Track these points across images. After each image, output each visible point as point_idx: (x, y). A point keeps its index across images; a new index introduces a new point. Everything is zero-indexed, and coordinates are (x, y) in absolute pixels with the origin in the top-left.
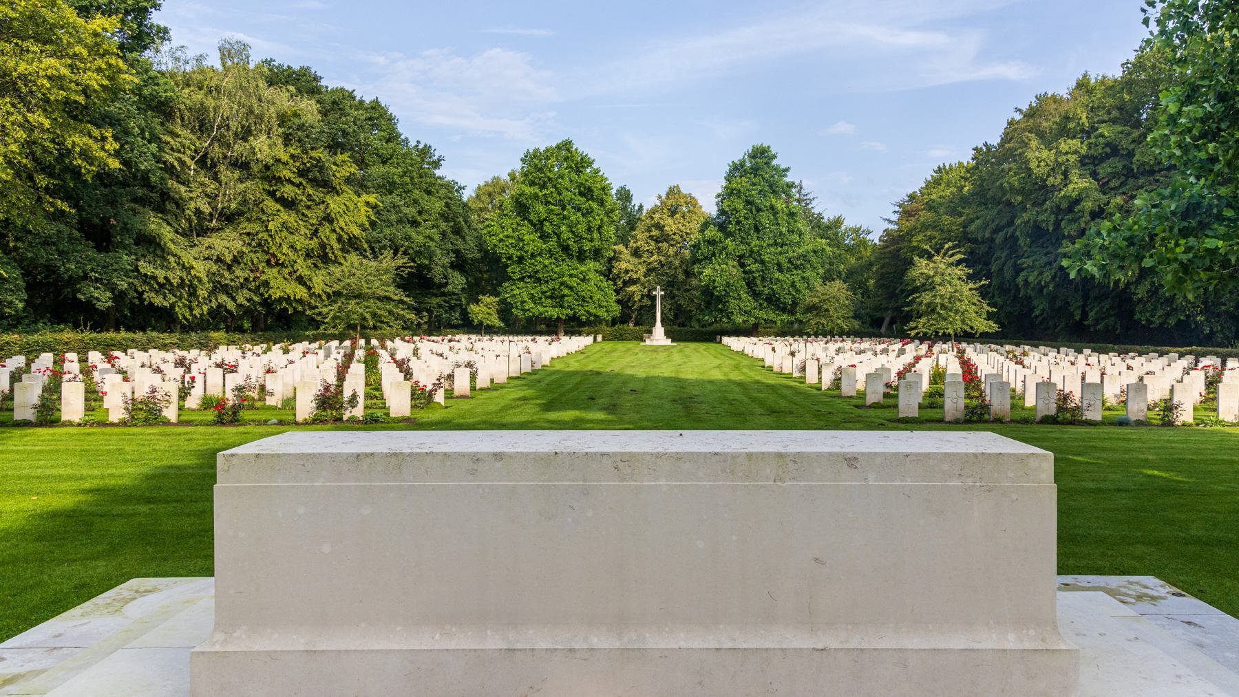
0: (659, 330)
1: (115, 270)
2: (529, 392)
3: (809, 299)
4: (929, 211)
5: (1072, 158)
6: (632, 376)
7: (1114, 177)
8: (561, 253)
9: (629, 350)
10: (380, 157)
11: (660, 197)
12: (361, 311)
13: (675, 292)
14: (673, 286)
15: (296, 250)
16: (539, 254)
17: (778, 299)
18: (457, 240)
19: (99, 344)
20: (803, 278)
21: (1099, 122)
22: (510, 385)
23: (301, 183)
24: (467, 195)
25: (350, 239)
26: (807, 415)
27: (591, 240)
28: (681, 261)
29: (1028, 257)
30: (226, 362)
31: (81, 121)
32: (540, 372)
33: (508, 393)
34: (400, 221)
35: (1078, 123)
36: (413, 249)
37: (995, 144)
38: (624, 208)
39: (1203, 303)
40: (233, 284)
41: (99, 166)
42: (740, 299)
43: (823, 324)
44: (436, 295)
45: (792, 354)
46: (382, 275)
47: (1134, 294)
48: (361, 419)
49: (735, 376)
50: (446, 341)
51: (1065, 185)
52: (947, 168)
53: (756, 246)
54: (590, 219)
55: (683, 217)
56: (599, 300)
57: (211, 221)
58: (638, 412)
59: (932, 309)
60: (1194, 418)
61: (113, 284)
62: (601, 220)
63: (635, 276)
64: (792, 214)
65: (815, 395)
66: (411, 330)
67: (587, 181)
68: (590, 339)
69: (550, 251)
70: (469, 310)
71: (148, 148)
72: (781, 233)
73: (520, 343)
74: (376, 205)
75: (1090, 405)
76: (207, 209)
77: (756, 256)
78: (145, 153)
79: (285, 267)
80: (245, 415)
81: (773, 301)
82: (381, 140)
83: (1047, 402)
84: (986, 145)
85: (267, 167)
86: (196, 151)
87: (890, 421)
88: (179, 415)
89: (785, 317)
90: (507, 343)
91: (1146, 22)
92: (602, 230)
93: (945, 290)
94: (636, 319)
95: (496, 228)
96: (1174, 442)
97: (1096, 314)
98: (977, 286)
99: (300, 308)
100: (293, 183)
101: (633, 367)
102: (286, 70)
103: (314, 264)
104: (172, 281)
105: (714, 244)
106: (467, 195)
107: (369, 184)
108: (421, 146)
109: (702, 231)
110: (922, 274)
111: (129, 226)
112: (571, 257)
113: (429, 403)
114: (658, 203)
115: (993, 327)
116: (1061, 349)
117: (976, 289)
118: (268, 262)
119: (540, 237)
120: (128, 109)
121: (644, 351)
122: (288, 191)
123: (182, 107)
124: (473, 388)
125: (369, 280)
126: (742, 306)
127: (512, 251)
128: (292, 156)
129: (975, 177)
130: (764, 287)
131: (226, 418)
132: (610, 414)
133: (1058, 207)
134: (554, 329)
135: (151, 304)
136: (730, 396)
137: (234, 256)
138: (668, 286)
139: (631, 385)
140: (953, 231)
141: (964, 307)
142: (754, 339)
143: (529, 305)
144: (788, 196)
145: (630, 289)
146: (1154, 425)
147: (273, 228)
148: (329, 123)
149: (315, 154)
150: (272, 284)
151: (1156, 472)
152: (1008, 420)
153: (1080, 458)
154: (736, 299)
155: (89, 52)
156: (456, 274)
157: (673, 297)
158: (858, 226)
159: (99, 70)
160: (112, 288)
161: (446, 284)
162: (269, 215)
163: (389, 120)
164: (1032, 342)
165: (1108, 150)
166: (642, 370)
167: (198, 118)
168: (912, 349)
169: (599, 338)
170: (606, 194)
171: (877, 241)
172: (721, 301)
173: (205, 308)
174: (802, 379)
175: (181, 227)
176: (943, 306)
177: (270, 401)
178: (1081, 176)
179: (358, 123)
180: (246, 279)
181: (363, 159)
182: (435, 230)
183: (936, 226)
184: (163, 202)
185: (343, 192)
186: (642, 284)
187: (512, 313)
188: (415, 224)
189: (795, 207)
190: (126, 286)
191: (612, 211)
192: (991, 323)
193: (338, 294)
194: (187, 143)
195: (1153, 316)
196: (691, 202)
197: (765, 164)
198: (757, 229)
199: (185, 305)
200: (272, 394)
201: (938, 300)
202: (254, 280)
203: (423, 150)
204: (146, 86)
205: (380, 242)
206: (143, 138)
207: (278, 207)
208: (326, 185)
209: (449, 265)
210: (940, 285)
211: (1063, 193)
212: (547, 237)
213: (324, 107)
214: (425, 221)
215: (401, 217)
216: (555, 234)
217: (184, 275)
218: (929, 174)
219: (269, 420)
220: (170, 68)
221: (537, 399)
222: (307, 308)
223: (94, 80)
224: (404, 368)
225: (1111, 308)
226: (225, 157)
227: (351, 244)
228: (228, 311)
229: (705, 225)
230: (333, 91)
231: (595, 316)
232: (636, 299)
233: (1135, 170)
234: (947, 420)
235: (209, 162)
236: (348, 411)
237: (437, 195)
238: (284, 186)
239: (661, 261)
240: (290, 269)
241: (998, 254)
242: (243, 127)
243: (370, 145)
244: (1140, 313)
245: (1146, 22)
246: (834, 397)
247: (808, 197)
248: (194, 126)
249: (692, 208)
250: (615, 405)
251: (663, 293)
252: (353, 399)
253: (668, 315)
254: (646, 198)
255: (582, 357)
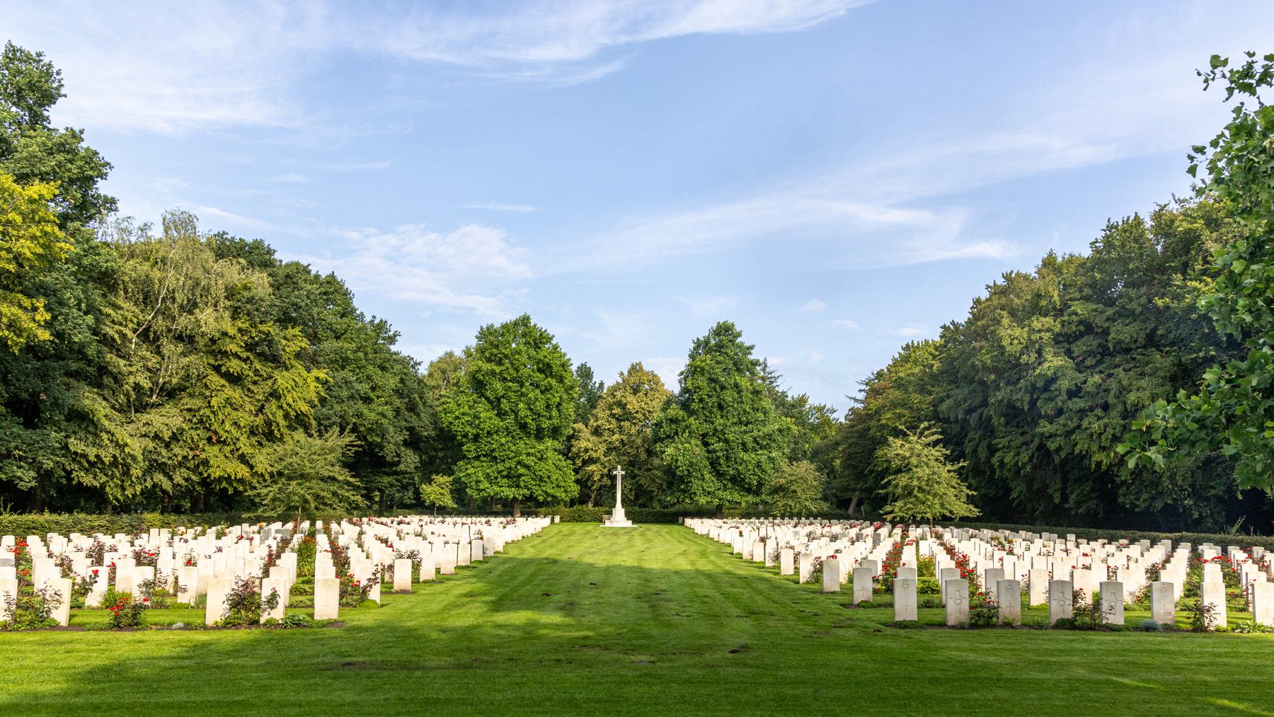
0: (619, 511)
1: (41, 448)
2: (479, 586)
3: (775, 480)
4: (898, 389)
5: (1046, 336)
6: (591, 565)
7: (1090, 356)
8: (518, 431)
9: (588, 532)
10: (334, 331)
11: (622, 374)
12: (302, 492)
13: (636, 472)
14: (633, 466)
15: (239, 427)
16: (496, 432)
17: (743, 480)
18: (411, 417)
19: (19, 527)
20: (769, 457)
21: (1071, 300)
22: (459, 576)
23: (248, 358)
24: (423, 371)
25: (298, 415)
26: (790, 617)
27: (550, 418)
28: (643, 440)
29: (1003, 437)
30: (147, 550)
31: (12, 291)
32: (491, 560)
33: (453, 587)
34: (352, 397)
35: (1050, 301)
36: (364, 426)
37: (963, 323)
38: (585, 386)
39: (1190, 486)
40: (170, 462)
41: (28, 337)
42: (703, 479)
43: (791, 506)
44: (388, 474)
45: (763, 540)
46: (328, 454)
47: (1117, 476)
48: (280, 622)
49: (703, 565)
50: (395, 523)
51: (1040, 364)
52: (916, 344)
53: (720, 425)
54: (549, 396)
55: (646, 395)
56: (557, 479)
57: (151, 396)
58: (598, 613)
59: (908, 492)
60: (1228, 622)
61: (39, 462)
62: (561, 397)
63: (594, 455)
64: (756, 392)
65: (794, 590)
66: (353, 511)
67: (545, 357)
68: (547, 521)
69: (507, 429)
70: (421, 491)
71: (84, 320)
72: (745, 412)
73: (473, 526)
74: (327, 381)
75: (1112, 608)
76: (146, 384)
77: (720, 435)
78: (80, 325)
79: (227, 445)
80: (150, 616)
81: (737, 481)
82: (335, 315)
83: (1062, 603)
84: (953, 323)
85: (213, 341)
86: (138, 324)
87: (885, 625)
88: (71, 616)
89: (751, 498)
90: (458, 526)
91: (1192, 171)
92: (561, 408)
93: (923, 472)
94: (595, 498)
95: (452, 405)
96: (1219, 655)
97: (1077, 496)
98: (955, 467)
99: (241, 488)
100: (239, 358)
101: (592, 553)
102: (238, 243)
103: (258, 441)
104: (104, 459)
105: (676, 423)
106: (423, 371)
107: (321, 359)
108: (377, 321)
109: (664, 410)
110: (898, 455)
111: (60, 401)
112: (528, 435)
113: (363, 601)
114: (620, 381)
115: (975, 512)
116: (1043, 534)
117: (954, 471)
118: (209, 440)
119: (498, 415)
120: (65, 280)
121: (603, 533)
122: (234, 366)
123: (126, 279)
124: (416, 581)
125: (313, 460)
126: (706, 487)
127: (468, 429)
128: (240, 330)
129: (944, 355)
130: (728, 466)
131: (124, 621)
132: (567, 615)
133: (1033, 386)
134: (510, 509)
135: (80, 483)
136: (700, 591)
137: (173, 433)
138: (629, 466)
139: (591, 578)
140: (923, 410)
141: (943, 490)
142: (719, 522)
143: (485, 485)
144: (753, 373)
145: (589, 468)
146: (1183, 630)
147: (216, 405)
148: (281, 297)
149: (263, 328)
150: (212, 462)
151: (1226, 702)
152: (1019, 623)
153: (1126, 681)
154: (699, 479)
155: (24, 219)
156: (409, 452)
157: (634, 477)
158: (822, 405)
159: (33, 238)
160: (35, 464)
161: (399, 462)
162: (213, 391)
163: (344, 294)
164: (1009, 526)
165: (1082, 328)
166: (602, 557)
167: (142, 290)
168: (888, 538)
169: (557, 519)
170: (565, 371)
171: (842, 420)
172: (683, 482)
173: (139, 488)
174: (776, 569)
175: (119, 402)
176: (920, 489)
177: (182, 599)
178: (1056, 354)
179: (312, 297)
180: (185, 458)
181: (316, 333)
182: (388, 407)
183: (905, 404)
184: (101, 376)
185: (292, 367)
186: (602, 464)
187: (466, 493)
188: (367, 400)
189: (760, 385)
190: (52, 465)
191: (572, 388)
192: (971, 507)
193: (280, 474)
194: (129, 315)
195: (1138, 499)
196: (654, 380)
197: (730, 341)
198: (721, 407)
199: (116, 486)
200: (185, 590)
201: (915, 483)
202: (193, 458)
203: (378, 325)
204: (86, 256)
205: (329, 419)
206: (80, 310)
207: (223, 382)
208: (274, 359)
209: (402, 443)
210: (916, 467)
211: (1038, 371)
212: (504, 415)
213: (277, 281)
214: (378, 397)
215: (352, 394)
216: (513, 411)
217: (117, 453)
218: (896, 351)
219: (174, 623)
220: (116, 239)
221: (486, 595)
222: (248, 487)
223: (26, 248)
224: (340, 560)
225: (1093, 490)
226: (169, 331)
227: (299, 421)
228: (164, 492)
229: (668, 403)
230: (287, 265)
231: (553, 496)
232: (595, 479)
233: (1112, 349)
234: (950, 623)
235: (152, 336)
236: (267, 613)
237: (391, 371)
238: (230, 360)
239: (622, 440)
240: (233, 447)
241: (971, 435)
242: (189, 300)
243: (324, 320)
244: (1124, 495)
245: (1192, 171)
246: (816, 592)
247: (773, 375)
248: (138, 299)
249: (654, 386)
250: (572, 604)
251: (623, 473)
252: (273, 599)
253: (629, 495)
254: (607, 376)
255: (537, 541)
